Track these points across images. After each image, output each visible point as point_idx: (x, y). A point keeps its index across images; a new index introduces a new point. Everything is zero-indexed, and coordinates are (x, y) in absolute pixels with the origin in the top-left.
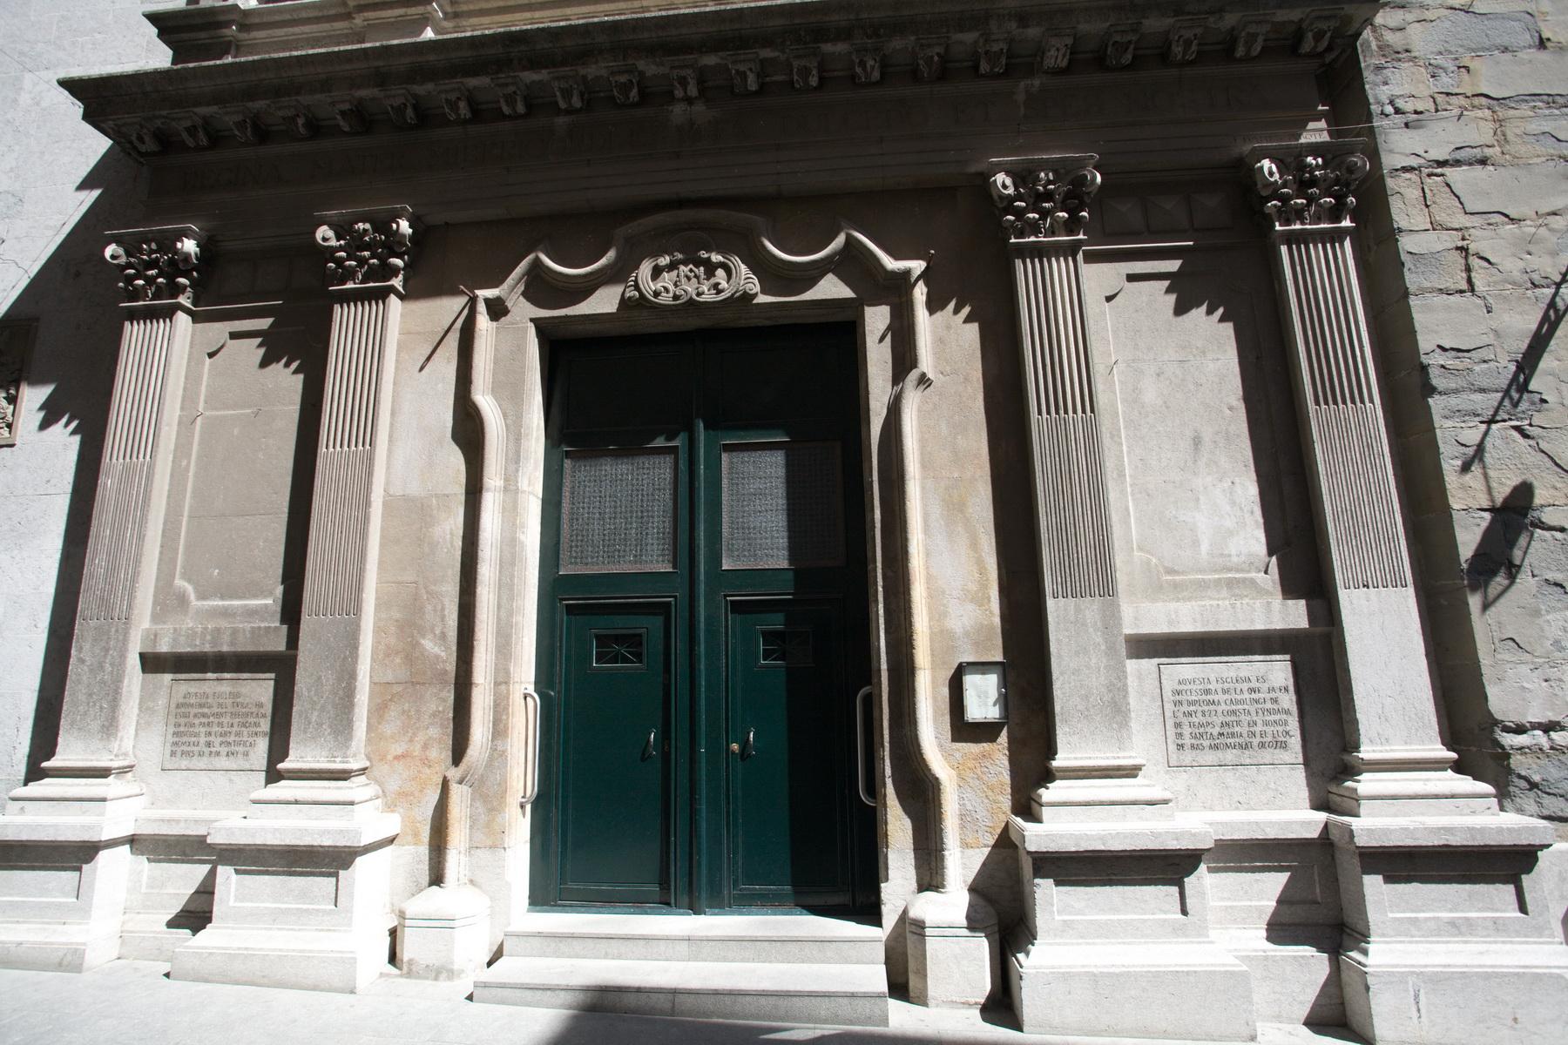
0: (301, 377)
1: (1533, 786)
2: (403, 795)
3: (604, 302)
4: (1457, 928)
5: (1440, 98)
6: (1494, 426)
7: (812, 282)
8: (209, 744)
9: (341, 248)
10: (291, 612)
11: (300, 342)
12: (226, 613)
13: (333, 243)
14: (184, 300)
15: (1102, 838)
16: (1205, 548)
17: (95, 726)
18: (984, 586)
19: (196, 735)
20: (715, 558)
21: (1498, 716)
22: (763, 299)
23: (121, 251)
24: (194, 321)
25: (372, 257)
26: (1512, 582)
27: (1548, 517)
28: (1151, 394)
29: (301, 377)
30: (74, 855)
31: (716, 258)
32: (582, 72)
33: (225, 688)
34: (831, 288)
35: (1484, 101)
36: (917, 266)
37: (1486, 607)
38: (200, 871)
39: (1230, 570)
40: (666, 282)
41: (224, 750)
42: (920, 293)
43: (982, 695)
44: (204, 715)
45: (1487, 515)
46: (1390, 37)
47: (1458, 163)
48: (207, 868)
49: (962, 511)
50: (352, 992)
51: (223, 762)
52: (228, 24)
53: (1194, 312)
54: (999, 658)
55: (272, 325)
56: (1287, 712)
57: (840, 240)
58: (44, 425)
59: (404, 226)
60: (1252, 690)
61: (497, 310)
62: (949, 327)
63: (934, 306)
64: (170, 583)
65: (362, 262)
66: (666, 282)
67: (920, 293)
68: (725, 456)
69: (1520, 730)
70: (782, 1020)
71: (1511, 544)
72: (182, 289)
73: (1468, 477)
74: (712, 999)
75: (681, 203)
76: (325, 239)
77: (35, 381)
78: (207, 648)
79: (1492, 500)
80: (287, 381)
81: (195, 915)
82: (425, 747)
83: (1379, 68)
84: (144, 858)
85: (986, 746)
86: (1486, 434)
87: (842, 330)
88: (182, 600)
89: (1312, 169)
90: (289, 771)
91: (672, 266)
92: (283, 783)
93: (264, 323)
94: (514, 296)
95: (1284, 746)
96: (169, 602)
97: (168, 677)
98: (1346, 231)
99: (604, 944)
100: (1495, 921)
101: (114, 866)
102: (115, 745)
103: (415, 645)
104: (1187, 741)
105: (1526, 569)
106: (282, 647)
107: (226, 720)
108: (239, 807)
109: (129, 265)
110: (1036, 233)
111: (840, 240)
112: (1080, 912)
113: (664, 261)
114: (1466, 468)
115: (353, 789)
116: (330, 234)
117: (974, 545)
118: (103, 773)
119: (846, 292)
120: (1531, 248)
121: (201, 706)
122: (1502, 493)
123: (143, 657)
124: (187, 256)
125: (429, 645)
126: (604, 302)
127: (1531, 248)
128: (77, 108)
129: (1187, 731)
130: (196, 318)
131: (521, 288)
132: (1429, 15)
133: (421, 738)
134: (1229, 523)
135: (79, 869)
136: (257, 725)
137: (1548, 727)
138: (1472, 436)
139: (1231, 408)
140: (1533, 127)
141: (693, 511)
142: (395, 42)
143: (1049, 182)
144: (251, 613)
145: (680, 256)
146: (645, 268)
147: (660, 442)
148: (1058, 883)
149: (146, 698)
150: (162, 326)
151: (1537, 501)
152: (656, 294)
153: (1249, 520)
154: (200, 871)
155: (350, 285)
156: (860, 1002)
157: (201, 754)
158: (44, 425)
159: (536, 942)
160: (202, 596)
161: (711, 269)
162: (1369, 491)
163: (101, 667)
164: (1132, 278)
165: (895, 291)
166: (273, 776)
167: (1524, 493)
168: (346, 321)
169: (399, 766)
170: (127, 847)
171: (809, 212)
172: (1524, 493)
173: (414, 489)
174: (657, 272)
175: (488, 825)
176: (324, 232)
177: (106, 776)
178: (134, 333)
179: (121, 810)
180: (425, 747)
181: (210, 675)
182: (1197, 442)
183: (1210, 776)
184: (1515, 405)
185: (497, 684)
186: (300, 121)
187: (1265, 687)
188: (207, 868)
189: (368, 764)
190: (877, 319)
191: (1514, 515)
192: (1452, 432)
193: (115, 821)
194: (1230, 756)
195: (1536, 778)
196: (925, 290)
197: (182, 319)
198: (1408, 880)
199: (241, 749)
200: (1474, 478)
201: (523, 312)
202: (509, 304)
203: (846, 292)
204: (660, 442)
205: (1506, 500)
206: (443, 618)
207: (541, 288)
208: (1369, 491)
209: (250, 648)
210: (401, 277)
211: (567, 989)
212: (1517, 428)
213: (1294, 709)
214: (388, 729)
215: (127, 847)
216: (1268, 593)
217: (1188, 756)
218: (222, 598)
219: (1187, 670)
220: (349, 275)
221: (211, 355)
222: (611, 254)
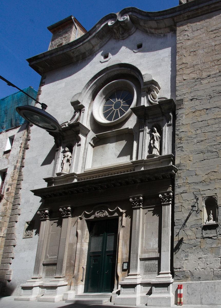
0: (158, 217)
1: (177, 276)
2: (68, 280)
3: (92, 217)
4: (161, 293)
5: (183, 183)
6: (181, 230)
7: (114, 214)
8: (49, 274)
9: (63, 211)
10: (160, 251)
11: (158, 212)
12: (52, 258)
13: (62, 211)
14: (141, 206)
15: (126, 283)
16: (151, 247)
17: (36, 273)
18: (127, 253)
19: (48, 273)
20: (105, 249)
21: (174, 267)
22: (109, 216)
23: (40, 212)
24: (143, 209)
25: (167, 199)
26: (179, 250)
27: (184, 242)
28: (148, 227)
29: (158, 217)
30: (133, 286)
31: (104, 211)
32: (126, 180)
33: (51, 268)
34: (116, 214)
35: (188, 183)
36: (124, 211)
37: (175, 254)
38: (150, 288)
39: (153, 249)
40: (98, 215)
41: (51, 275)
42: (124, 215)
43: (125, 266)
44: (49, 271)
45: (178, 242)
46: (179, 175)
47: (183, 193)
48: (150, 287)
49: (126, 243)
50: (54, 302)
51: (51, 277)
52: (53, 179)
53: (155, 215)
54: (128, 261)
55: (58, 221)
56: (157, 267)
57: (116, 208)
58: (36, 235)
59: (141, 198)
60: (153, 265)
61: (81, 219)
62: (128, 219)
63: (126, 216)
64: (46, 255)
65: (65, 213)
66: (98, 215)
67: (124, 215)
68: (108, 236)
69: (176, 269)
70: (88, 303)
71: (180, 245)
72: (141, 204)
73: (176, 237)
74: (82, 301)
75: (101, 203)
76: (160, 196)
77: (35, 229)
78: (49, 263)
79: (178, 240)
80: (156, 217)
81: (150, 293)
82: (71, 274)
83: (177, 179)
84: (142, 286)
85: (125, 272)
86: (179, 231)
87: (116, 219)
88: (48, 257)
89: (165, 195)
90: (129, 275)
91: (99, 212)
92: (160, 275)
93: (153, 209)
94: (83, 217)
95: (156, 271)
96: (46, 257)
97: (46, 266)
98: (170, 203)
99: (85, 297)
100: (164, 292)
101: (139, 287)
102: (62, 274)
103: (71, 261)
104: (146, 271)
105: (181, 248)
106: (159, 256)
107: (51, 271)
108: (154, 279)
109: (41, 214)
110: (165, 202)
111: (116, 208)
112: (125, 291)
113: (98, 211)
114: (176, 236)
115: (138, 277)
116: (61, 209)
117: (127, 247)
118: (136, 275)
119: (117, 215)
120: (189, 205)
121: (49, 270)
122: (180, 239)
123: (140, 259)
124: (47, 213)
125: (72, 261)
126: (92, 217)
127: (189, 205)
128: (33, 193)
129: (146, 270)
130: (143, 208)
131: (84, 215)
132: (184, 171)
133: (70, 273)
134: (154, 243)
135: (168, 287)
136: (54, 272)
137: (180, 268)
138: (178, 231)
139: (157, 228)
140: (193, 187)
141: (104, 244)
142: (64, 184)
143: (136, 199)
144: (55, 258)
145: (100, 211)
146: (96, 213)
147: (101, 235)
148: (123, 288)
149: (44, 269)
150: (45, 222)
151: (183, 240)
152: (97, 216)
153: (157, 243)
154: (150, 288)
155: (64, 216)
156: (100, 302)
157: (49, 276)
158: (36, 235)
159: (78, 296)
160: (50, 256)
161: (103, 212)
162: (167, 239)
163: (37, 265)
164: (148, 211)
165: (121, 214)
166: (159, 274)
167: (182, 238)
168: (64, 220)
169: (68, 276)
170: (140, 285)
171: (113, 204)
172: (182, 238)
173: (72, 242)
174: (98, 213)
175: (76, 283)
176: (160, 195)
177: (136, 275)
178: (42, 223)
179: (139, 280)
180: (71, 274)
181: (50, 266)
182: (153, 233)
183: (148, 275)
184: (183, 227)
185: (79, 266)
186: (58, 194)
187: (155, 264)
188: (150, 287)
189: (65, 276)
190: (120, 218)
191: (181, 241)
192: (176, 231)
193: (139, 281)
194: (150, 273)
195: (177, 275)
196: (125, 214)
197: (47, 221)
198: (157, 287)
199: (52, 275)
200: (177, 237)
201: (84, 218)
202: (82, 218)
203: (117, 215)
204: (101, 235)
205: (180, 240)
206: (74, 258)
207: (86, 216)
208: (167, 239)
209: (53, 263)
210: (142, 205)
211: (74, 301)
212: (183, 230)
213: (158, 267)
214: (67, 272)
215: (140, 285)
216: (157, 252)
217: (146, 273)
218: (52, 256)
219: (147, 262)
220: (64, 215)
221: (146, 214)
222: (92, 211)
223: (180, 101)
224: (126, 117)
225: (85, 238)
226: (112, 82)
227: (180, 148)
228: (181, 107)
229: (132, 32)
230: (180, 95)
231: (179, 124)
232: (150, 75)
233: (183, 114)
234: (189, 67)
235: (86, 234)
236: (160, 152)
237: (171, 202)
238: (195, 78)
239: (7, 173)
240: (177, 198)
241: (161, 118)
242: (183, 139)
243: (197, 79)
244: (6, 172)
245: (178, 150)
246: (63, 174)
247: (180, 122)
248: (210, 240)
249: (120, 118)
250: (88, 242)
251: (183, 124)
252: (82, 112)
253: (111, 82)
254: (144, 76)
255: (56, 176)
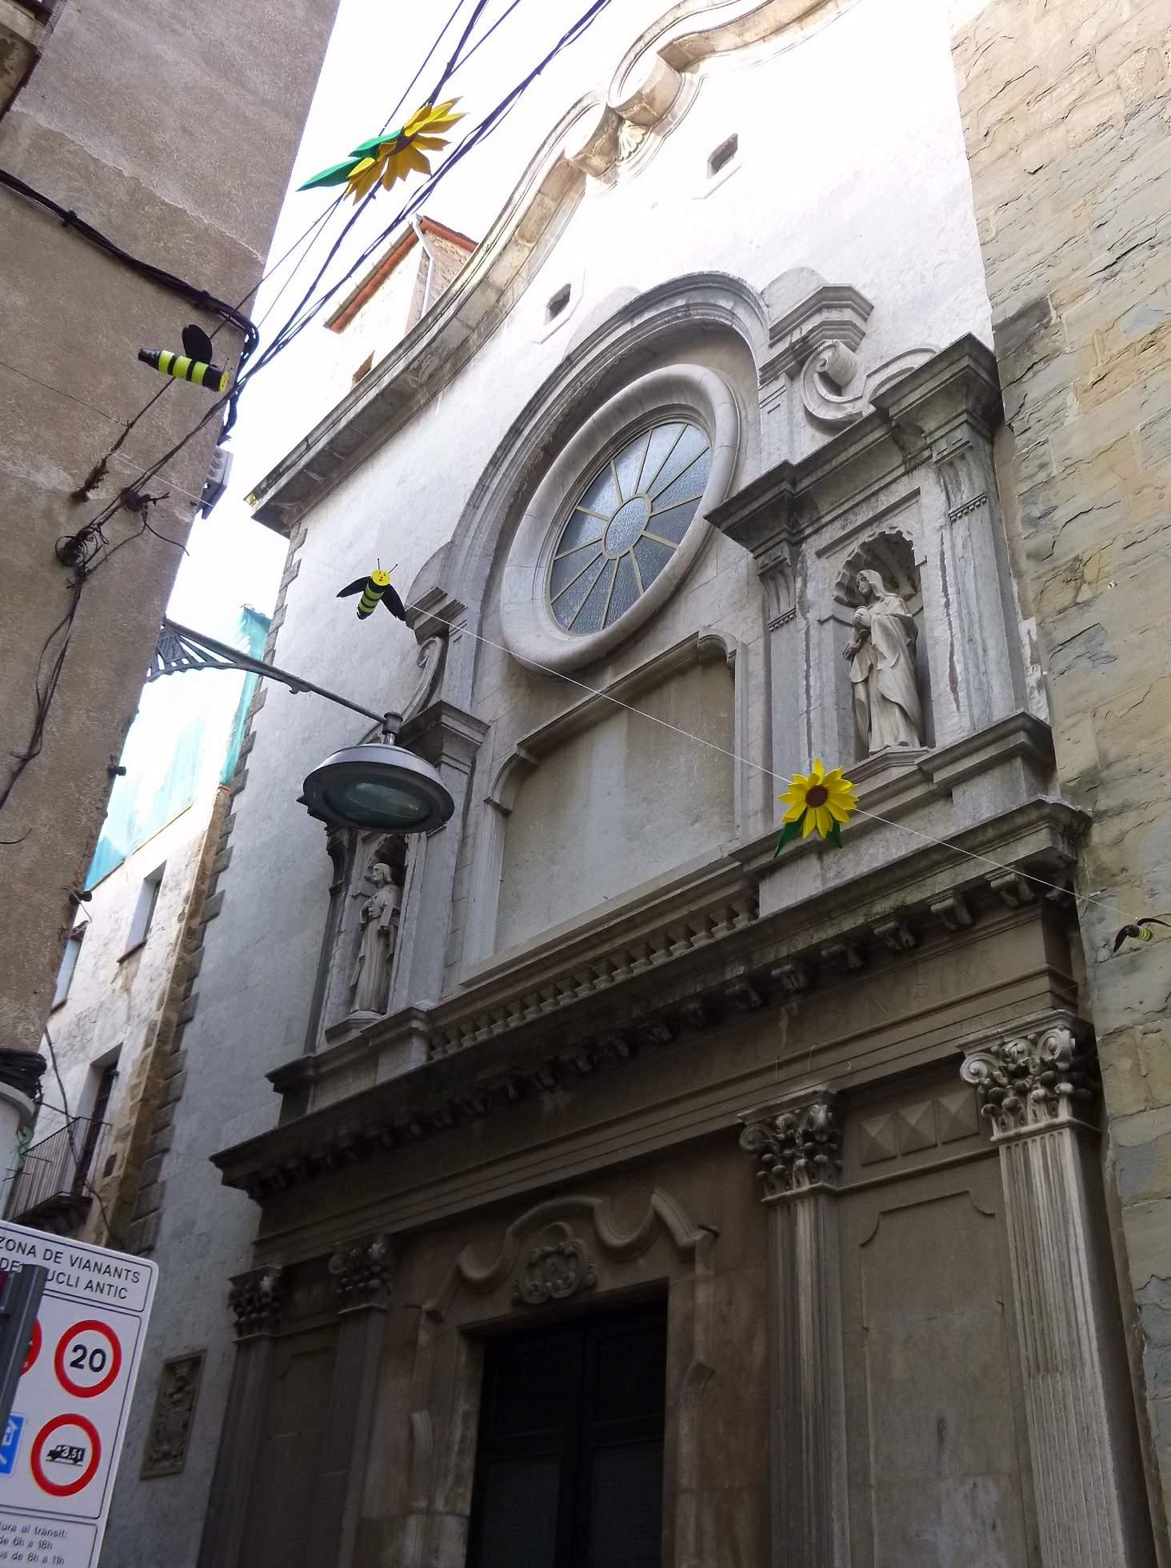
75: (552, 1191)
223: (1022, 322)
224: (680, 571)
225: (451, 1479)
226: (595, 415)
227: (1078, 648)
228: (1035, 358)
229: (680, 115)
230: (1014, 284)
231: (1042, 476)
232: (803, 269)
233: (1061, 389)
234: (1051, 81)
235: (456, 1448)
236: (921, 723)
237: (1064, 1114)
238: (1111, 118)
239: (119, 1068)
240: (1126, 1064)
241: (902, 489)
242: (1090, 573)
243: (1129, 118)
244: (115, 1064)
245: (1062, 666)
246: (358, 1023)
247: (1045, 459)
248: (1141, 1076)
249: (643, 596)
250: (467, 1511)
251: (1072, 466)
252: (452, 639)
253: (589, 421)
254: (766, 295)
255: (323, 1046)
